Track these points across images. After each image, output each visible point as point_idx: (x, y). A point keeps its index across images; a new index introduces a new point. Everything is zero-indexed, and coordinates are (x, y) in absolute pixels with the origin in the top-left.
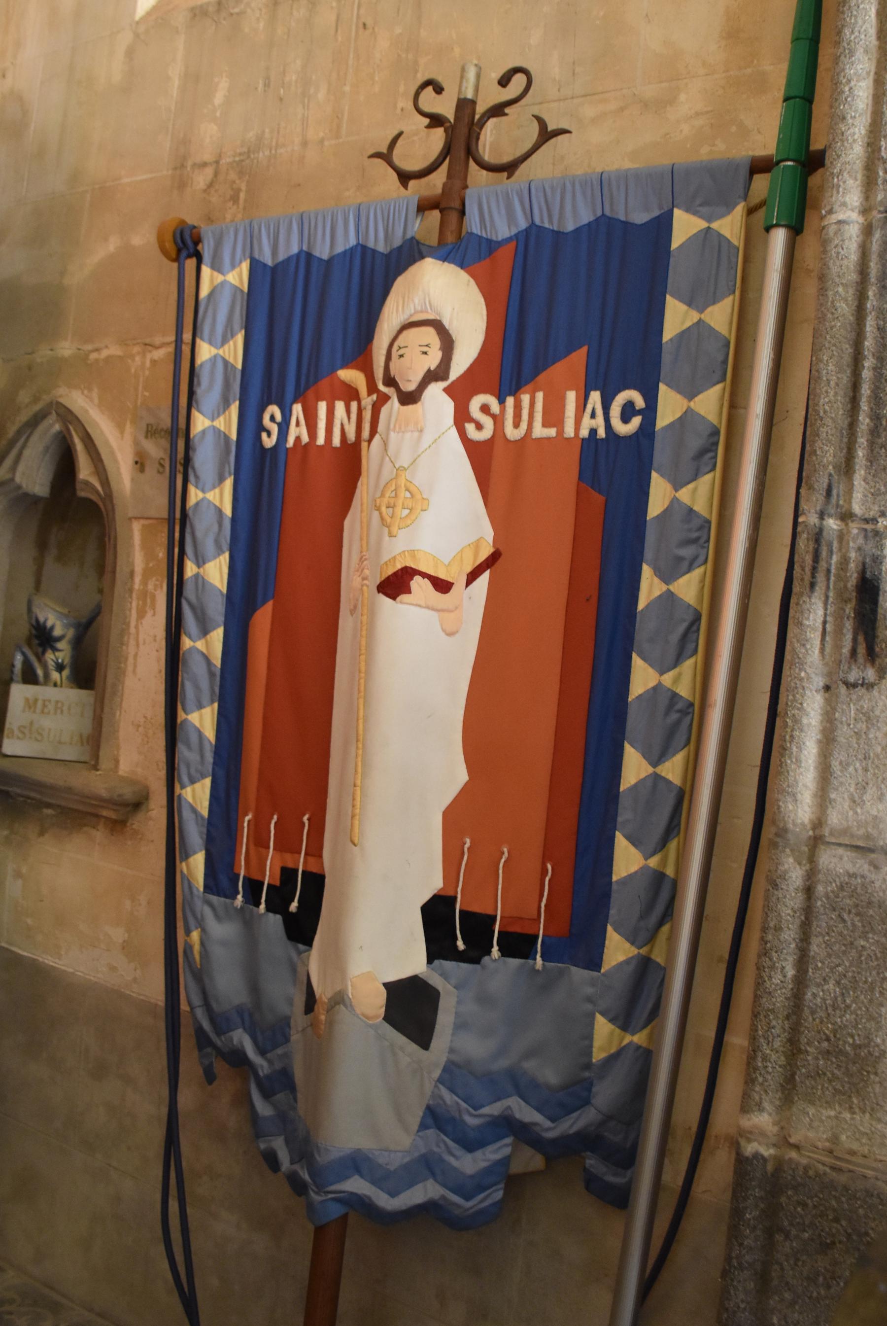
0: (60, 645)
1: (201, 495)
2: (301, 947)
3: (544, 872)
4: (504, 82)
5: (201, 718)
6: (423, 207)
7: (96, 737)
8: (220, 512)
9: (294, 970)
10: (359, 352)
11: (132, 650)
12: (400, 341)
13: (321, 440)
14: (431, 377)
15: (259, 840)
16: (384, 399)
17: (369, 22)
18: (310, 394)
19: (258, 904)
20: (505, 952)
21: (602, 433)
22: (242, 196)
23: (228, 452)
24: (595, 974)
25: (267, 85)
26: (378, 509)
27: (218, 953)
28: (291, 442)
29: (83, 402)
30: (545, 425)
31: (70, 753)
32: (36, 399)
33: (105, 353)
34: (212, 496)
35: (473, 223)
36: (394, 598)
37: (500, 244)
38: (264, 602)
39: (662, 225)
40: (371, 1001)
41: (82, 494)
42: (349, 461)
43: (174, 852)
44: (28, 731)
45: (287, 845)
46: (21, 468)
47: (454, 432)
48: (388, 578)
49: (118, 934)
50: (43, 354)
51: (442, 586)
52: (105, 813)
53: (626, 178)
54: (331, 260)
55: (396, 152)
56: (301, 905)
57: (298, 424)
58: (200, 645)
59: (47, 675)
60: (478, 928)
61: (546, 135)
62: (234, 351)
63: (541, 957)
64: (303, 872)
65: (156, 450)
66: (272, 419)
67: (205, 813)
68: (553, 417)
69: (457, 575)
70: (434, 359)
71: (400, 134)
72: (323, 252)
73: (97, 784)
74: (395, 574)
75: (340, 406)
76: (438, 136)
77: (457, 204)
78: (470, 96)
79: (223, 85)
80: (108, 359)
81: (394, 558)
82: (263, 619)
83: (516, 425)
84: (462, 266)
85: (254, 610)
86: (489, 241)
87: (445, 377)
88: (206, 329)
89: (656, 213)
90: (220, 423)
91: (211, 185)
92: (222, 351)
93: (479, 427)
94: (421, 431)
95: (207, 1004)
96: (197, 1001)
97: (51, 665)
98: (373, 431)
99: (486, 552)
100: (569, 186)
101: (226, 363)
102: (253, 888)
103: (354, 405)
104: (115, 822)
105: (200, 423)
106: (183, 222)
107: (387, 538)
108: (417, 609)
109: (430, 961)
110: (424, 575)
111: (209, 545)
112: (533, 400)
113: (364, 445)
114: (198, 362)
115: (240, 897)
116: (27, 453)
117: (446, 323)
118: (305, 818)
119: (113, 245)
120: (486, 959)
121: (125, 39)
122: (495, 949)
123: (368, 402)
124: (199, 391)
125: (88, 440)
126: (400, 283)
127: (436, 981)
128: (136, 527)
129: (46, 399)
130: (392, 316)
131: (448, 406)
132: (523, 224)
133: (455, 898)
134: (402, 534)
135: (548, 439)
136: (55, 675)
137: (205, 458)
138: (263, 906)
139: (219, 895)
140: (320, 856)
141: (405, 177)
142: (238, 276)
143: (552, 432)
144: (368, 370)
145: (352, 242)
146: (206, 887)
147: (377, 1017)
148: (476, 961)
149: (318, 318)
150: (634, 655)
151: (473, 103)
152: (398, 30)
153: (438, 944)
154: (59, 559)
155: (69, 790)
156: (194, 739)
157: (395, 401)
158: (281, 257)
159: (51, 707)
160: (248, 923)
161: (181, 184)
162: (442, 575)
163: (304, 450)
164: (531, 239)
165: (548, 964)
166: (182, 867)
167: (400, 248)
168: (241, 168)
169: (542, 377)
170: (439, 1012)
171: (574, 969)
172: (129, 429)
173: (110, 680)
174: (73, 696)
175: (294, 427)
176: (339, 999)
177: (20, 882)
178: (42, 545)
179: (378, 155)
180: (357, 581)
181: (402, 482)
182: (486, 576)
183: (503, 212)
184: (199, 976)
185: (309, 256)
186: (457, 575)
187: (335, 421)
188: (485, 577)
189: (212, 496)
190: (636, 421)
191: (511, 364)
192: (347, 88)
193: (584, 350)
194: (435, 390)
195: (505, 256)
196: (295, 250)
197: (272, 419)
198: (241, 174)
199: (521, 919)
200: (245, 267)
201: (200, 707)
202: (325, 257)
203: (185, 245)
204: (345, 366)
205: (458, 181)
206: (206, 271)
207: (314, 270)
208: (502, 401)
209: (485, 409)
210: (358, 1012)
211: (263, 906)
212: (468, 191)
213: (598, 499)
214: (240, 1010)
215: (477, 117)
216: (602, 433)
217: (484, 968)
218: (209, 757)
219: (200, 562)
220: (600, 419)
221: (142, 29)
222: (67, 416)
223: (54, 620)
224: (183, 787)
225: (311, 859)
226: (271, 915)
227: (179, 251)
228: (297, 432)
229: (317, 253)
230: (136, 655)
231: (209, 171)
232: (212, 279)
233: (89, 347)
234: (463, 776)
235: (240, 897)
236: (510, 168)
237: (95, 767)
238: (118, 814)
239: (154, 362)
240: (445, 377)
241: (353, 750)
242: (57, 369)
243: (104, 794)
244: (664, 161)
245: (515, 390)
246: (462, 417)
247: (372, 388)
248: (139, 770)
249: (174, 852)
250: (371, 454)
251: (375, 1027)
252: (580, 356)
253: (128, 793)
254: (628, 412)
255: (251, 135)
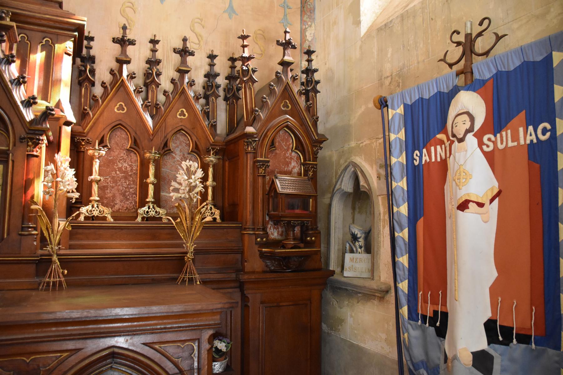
0: (360, 240)
1: (396, 184)
2: (442, 339)
3: (532, 310)
4: (481, 24)
5: (403, 260)
6: (458, 74)
7: (373, 269)
8: (403, 189)
9: (439, 347)
10: (443, 128)
11: (382, 239)
12: (455, 121)
13: (433, 160)
14: (468, 131)
15: (425, 301)
16: (453, 142)
17: (433, 18)
18: (428, 145)
19: (426, 324)
20: (519, 341)
21: (535, 141)
22: (401, 84)
23: (404, 169)
24: (558, 352)
25: (404, 47)
26: (455, 180)
27: (413, 341)
28: (423, 162)
29: (359, 160)
30: (513, 141)
31: (365, 275)
32: (346, 161)
33: (364, 143)
34: (400, 184)
35: (476, 76)
36: (463, 211)
37: (487, 80)
38: (420, 218)
39: (549, 58)
40: (468, 359)
41: (362, 190)
42: (443, 165)
43: (398, 307)
44: (351, 268)
45: (434, 302)
46: (343, 184)
47: (478, 149)
48: (460, 204)
49: (384, 336)
50: (346, 147)
51: (481, 205)
52: (377, 295)
53: (530, 46)
54: (430, 98)
55: (447, 58)
56: (440, 324)
57: (425, 156)
58: (401, 234)
59: (357, 250)
60: (507, 332)
61: (499, 38)
62: (402, 135)
63: (535, 344)
64: (441, 312)
65: (383, 172)
66: (417, 155)
67: (407, 292)
68: (515, 138)
69: (486, 201)
70: (468, 125)
71: (447, 51)
72: (426, 96)
73: (374, 285)
74: (463, 202)
75: (438, 147)
76: (461, 48)
77: (470, 70)
78: (469, 32)
79: (390, 50)
80: (365, 145)
81: (462, 197)
82: (420, 223)
83: (502, 143)
84: (474, 91)
85: (417, 221)
86: (483, 80)
87: (473, 131)
88: (392, 129)
89: (545, 55)
90: (400, 159)
91: (390, 83)
92: (398, 136)
93: (488, 146)
94: (466, 151)
95: (411, 360)
96: (408, 359)
97: (358, 246)
98: (450, 154)
99: (496, 191)
100: (509, 54)
101: (400, 139)
102: (424, 318)
103: (443, 146)
104: (381, 297)
105: (394, 160)
106: (381, 96)
107: (458, 190)
108: (472, 214)
109: (489, 344)
110: (473, 202)
111: (400, 201)
112: (507, 134)
113: (448, 159)
114: (391, 140)
115: (420, 321)
116: (344, 179)
117: (471, 112)
118: (440, 292)
119: (363, 108)
120: (511, 344)
121: (359, 43)
122: (515, 340)
123: (447, 144)
124: (392, 150)
125: (362, 172)
126: (453, 102)
127: (492, 352)
128: (380, 198)
129: (349, 161)
130: (452, 113)
131: (475, 141)
132: (494, 72)
133: (497, 320)
134: (464, 188)
135: (514, 146)
136: (359, 250)
137: (397, 172)
138: (427, 324)
139: (413, 321)
140: (446, 306)
141: (451, 65)
142: (400, 110)
143: (516, 144)
144: (446, 133)
145: (436, 91)
146: (409, 318)
147: (469, 365)
148: (507, 345)
149: (428, 119)
150: (559, 223)
151: (471, 34)
152: (443, 17)
153: (492, 337)
154: (359, 212)
155: (365, 287)
156: (401, 267)
157: (456, 142)
158: (413, 101)
159: (358, 260)
160: (424, 331)
161: (381, 85)
162: (480, 201)
163: (428, 164)
164: (498, 76)
165: (538, 347)
166: (400, 311)
167: (452, 90)
168: (399, 75)
169: (509, 125)
170: (494, 364)
171: (549, 350)
172: (374, 166)
173: (376, 249)
174: (365, 256)
175: (424, 157)
176: (455, 358)
177: (352, 319)
178: (354, 209)
179: (441, 60)
180: (450, 207)
181: (462, 170)
182: (497, 199)
183: (486, 68)
184: (408, 350)
185: (422, 99)
186: (486, 201)
187: (437, 153)
188: (497, 200)
189: (400, 184)
190: (548, 134)
191: (497, 122)
192: (429, 41)
193: (524, 111)
194: (470, 136)
195: (489, 85)
196: (417, 98)
197: (417, 155)
198: (399, 77)
199: (525, 329)
200: (402, 106)
201: (402, 256)
202: (427, 98)
203: (383, 104)
204: (439, 133)
205: (469, 62)
206: (390, 110)
207: (424, 103)
208: (495, 136)
209: (489, 140)
210: (462, 362)
211: (427, 324)
212: (473, 65)
213: (537, 166)
214: (422, 362)
215: (473, 37)
216: (535, 141)
217: (511, 347)
218: (407, 273)
219: (398, 206)
220: (534, 136)
221: (363, 40)
222: (355, 165)
223: (357, 231)
224: (399, 283)
225: (443, 307)
226: (430, 327)
227: (381, 106)
228: (425, 158)
229: (425, 97)
230: (383, 241)
231: (389, 79)
232: (392, 113)
233: (360, 142)
234: (495, 274)
235: (420, 321)
236: (487, 53)
237: (373, 279)
238: (380, 295)
239: (380, 144)
240: (472, 131)
241: (454, 266)
242: (351, 151)
243: (375, 288)
244: (546, 35)
245: (500, 131)
246: (481, 144)
247: (448, 139)
248: (387, 280)
249: (398, 307)
250: (450, 162)
251: (469, 369)
252: (522, 115)
253: (383, 287)
254: (544, 131)
255: (401, 64)
